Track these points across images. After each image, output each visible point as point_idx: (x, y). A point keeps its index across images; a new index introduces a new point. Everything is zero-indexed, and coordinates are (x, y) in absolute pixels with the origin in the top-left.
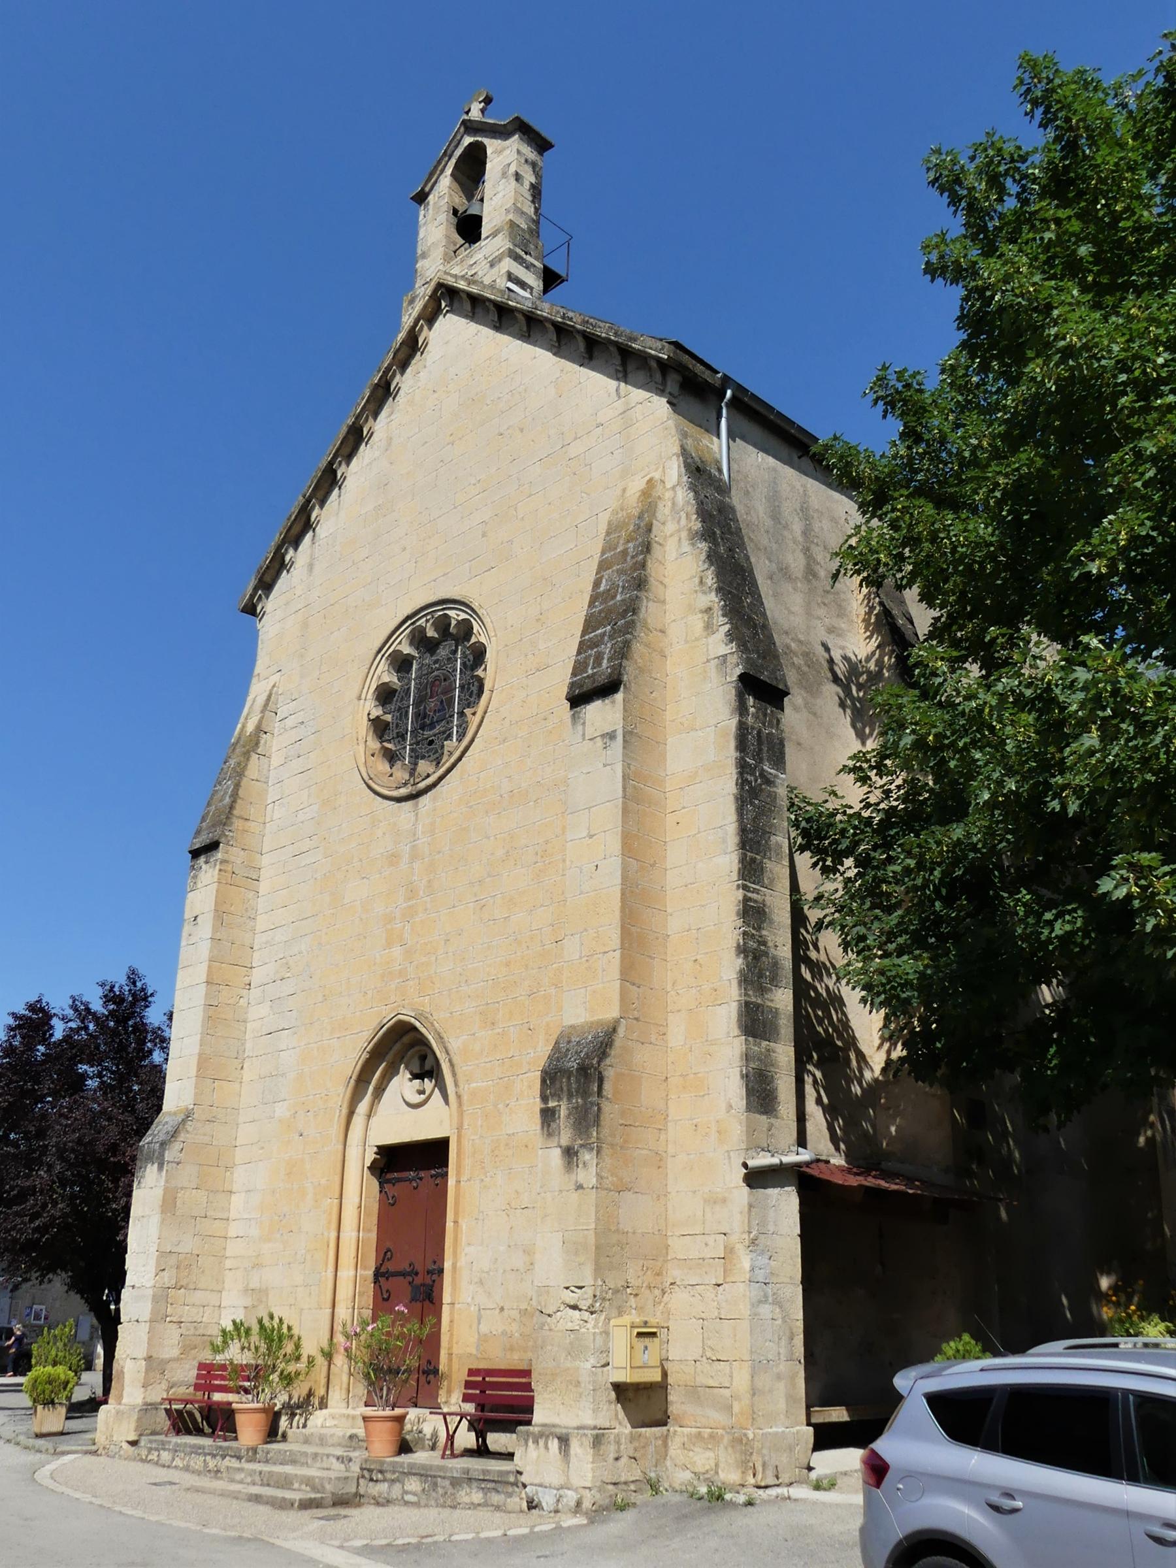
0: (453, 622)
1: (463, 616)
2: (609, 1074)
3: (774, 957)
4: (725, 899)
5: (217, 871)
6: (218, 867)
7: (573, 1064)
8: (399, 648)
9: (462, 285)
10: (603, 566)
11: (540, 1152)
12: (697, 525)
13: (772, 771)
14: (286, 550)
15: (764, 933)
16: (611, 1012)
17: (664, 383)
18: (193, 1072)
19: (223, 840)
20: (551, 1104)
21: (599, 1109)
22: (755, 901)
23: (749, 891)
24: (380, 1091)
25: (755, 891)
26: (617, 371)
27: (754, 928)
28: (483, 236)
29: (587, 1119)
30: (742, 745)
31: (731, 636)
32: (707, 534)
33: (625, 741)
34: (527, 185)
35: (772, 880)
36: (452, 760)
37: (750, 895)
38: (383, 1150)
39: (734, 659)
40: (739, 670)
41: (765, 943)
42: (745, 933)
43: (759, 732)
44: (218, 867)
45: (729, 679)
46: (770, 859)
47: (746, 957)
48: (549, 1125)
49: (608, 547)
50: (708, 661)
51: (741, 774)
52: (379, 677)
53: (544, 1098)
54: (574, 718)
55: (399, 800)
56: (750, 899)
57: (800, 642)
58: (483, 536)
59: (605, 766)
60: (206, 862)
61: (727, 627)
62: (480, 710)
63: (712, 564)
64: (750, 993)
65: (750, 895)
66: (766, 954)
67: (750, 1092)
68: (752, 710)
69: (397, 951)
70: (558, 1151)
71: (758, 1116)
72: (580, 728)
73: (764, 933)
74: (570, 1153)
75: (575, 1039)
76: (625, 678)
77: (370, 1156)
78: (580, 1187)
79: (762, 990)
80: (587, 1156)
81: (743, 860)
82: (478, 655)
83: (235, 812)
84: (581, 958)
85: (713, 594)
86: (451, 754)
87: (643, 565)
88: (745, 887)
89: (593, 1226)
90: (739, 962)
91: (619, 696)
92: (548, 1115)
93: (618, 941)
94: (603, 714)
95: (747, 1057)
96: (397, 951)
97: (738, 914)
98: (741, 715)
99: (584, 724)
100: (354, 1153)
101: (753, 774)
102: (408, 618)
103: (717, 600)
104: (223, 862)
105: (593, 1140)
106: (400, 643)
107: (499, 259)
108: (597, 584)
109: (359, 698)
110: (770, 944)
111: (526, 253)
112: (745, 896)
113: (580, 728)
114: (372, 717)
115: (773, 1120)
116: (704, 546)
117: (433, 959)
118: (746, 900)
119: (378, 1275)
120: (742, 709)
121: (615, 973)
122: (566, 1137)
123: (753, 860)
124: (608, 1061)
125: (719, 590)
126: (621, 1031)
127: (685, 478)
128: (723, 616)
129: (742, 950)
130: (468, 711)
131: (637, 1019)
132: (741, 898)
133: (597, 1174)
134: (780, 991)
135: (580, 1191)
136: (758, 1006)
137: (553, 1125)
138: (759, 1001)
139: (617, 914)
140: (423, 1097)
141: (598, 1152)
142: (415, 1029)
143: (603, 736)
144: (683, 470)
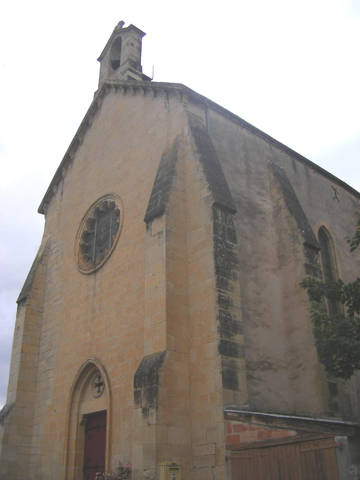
0: (109, 203)
1: (112, 200)
2: (161, 374)
3: (234, 321)
4: (212, 296)
5: (25, 309)
6: (26, 307)
7: (147, 371)
8: (90, 217)
9: (112, 82)
10: (160, 169)
11: (134, 410)
12: (195, 148)
13: (231, 243)
14: (54, 188)
15: (229, 310)
16: (163, 349)
17: (181, 99)
18: (16, 388)
19: (28, 297)
20: (138, 389)
21: (157, 390)
22: (224, 297)
23: (221, 292)
24: (84, 391)
25: (225, 293)
26: (165, 99)
27: (224, 308)
28: (120, 65)
29: (152, 394)
30: (216, 231)
31: (210, 189)
32: (200, 151)
33: (167, 234)
34: (135, 47)
35: (232, 288)
36: (108, 256)
37: (221, 294)
38: (85, 416)
39: (211, 197)
40: (213, 202)
41: (230, 315)
42: (220, 310)
43: (224, 227)
44: (26, 307)
45: (209, 206)
46: (231, 279)
47: (220, 321)
48: (137, 398)
49: (162, 161)
50: (201, 200)
51: (215, 244)
52: (83, 229)
53: (135, 387)
54: (148, 228)
55: (89, 274)
56: (222, 296)
57: (246, 198)
58: (119, 169)
59: (159, 245)
60: (22, 306)
61: (208, 185)
62: (117, 235)
63: (201, 162)
64: (223, 336)
65: (221, 294)
66: (230, 319)
67: (224, 380)
68: (220, 218)
69: (88, 334)
70: (140, 410)
71: (228, 390)
72: (150, 232)
73: (229, 310)
74: (145, 411)
75: (148, 361)
76: (166, 209)
77: (81, 419)
78: (149, 424)
79: (229, 335)
80: (153, 411)
81: (218, 279)
82: (118, 213)
83: (33, 286)
84: (151, 326)
85: (202, 173)
86: (107, 254)
87: (174, 166)
88: (219, 291)
89: (154, 442)
90: (218, 323)
91: (164, 217)
92: (137, 394)
93: (165, 318)
94: (159, 225)
95: (223, 364)
96: (88, 334)
97: (217, 302)
98: (215, 220)
99: (151, 230)
100: (74, 418)
101: (221, 244)
102: (93, 204)
103: (204, 175)
104: (28, 305)
105: (155, 403)
106: (91, 215)
107: (125, 72)
108: (157, 176)
109: (76, 238)
110: (232, 315)
111: (135, 69)
112: (219, 294)
113: (150, 232)
114: (81, 244)
115: (236, 392)
116: (198, 156)
117: (101, 336)
118: (220, 296)
119: (84, 468)
120: (215, 216)
121: (164, 330)
122: (144, 403)
123: (222, 280)
124: (161, 369)
125: (204, 172)
126: (167, 356)
127: (191, 132)
128: (206, 181)
129: (219, 318)
130: (113, 237)
131: (175, 351)
132: (217, 295)
133: (156, 418)
134: (238, 335)
135: (149, 426)
136: (227, 342)
137: (139, 399)
138: (228, 340)
139: (165, 306)
140: (99, 394)
141: (156, 408)
142: (95, 366)
143: (158, 233)
144: (190, 129)
